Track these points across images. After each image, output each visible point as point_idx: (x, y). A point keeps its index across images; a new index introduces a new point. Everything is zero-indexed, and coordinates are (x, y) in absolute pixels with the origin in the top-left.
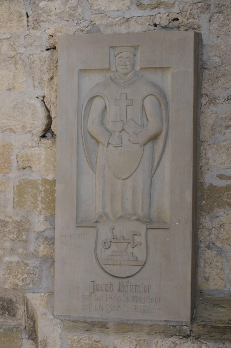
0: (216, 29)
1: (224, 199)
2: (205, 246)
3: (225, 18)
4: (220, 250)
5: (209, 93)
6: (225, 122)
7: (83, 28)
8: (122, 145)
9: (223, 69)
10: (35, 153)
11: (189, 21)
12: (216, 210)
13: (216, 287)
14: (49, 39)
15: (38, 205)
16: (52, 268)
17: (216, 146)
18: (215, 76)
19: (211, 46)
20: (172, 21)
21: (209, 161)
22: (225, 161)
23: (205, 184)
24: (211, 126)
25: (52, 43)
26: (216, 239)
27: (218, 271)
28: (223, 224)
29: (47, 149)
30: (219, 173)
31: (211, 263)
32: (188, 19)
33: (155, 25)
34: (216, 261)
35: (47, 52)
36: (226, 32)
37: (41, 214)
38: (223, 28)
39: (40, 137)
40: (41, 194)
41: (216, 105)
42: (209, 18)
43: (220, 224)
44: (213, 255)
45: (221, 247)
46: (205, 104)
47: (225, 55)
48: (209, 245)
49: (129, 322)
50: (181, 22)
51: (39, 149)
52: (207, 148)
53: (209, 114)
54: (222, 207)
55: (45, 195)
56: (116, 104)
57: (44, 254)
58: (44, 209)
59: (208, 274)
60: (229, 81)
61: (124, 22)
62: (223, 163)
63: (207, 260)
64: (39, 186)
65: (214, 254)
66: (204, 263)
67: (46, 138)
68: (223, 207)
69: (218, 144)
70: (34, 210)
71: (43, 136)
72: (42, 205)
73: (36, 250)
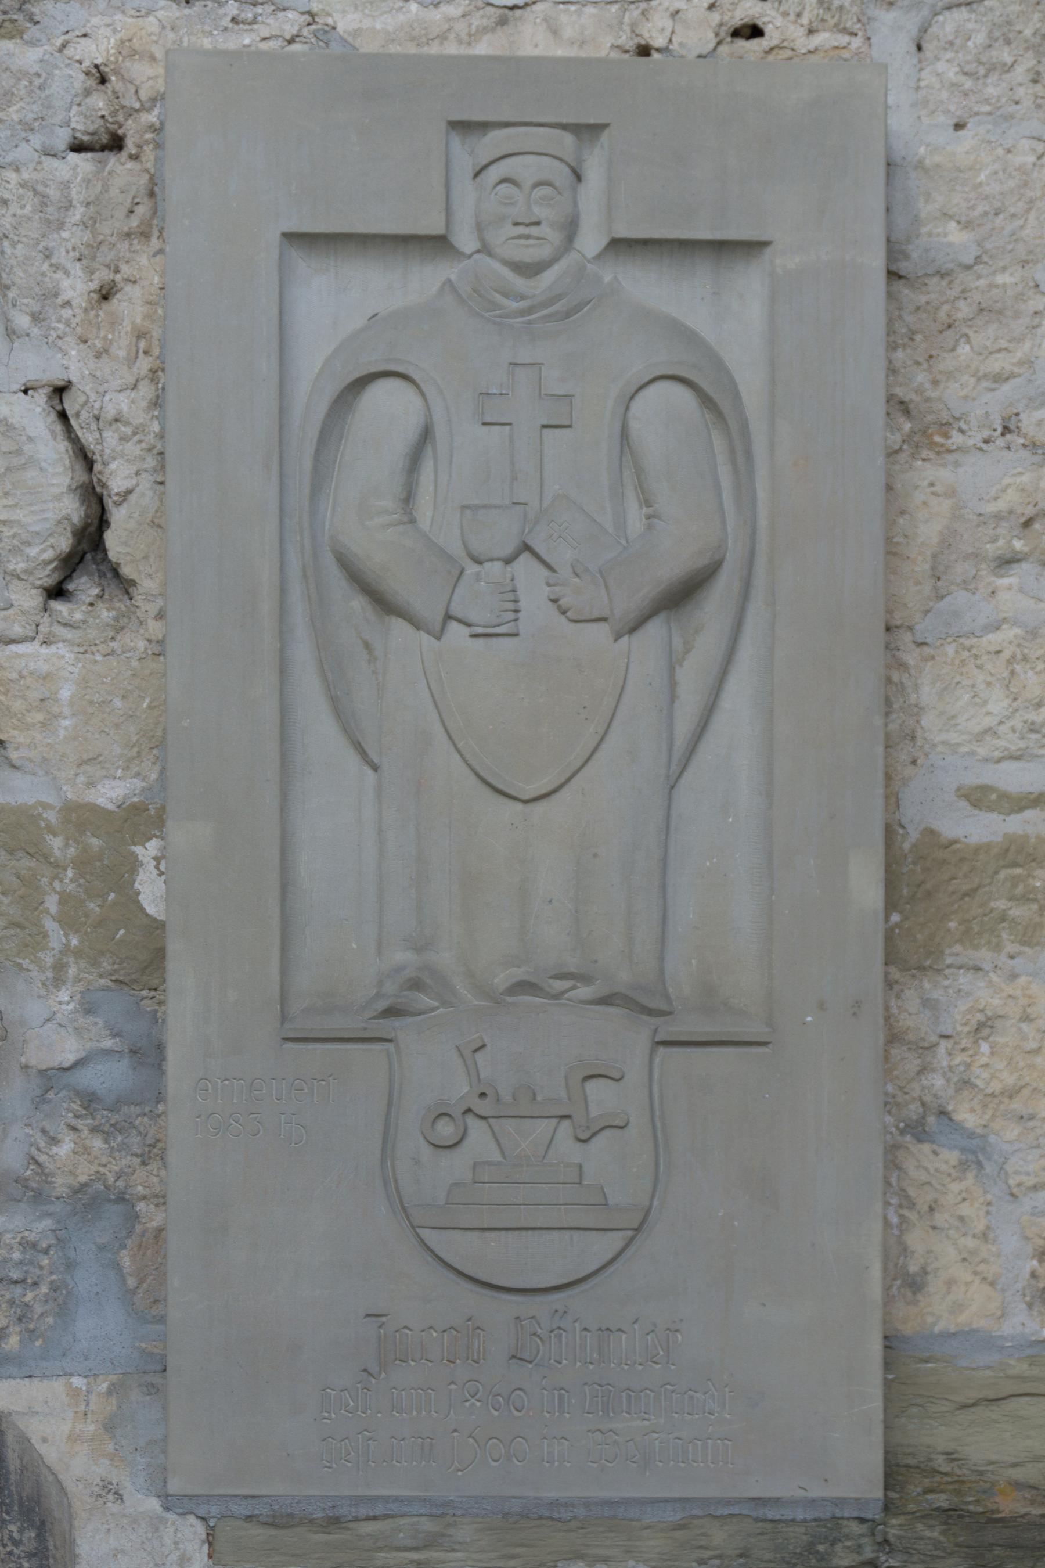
0: (953, 85)
1: (992, 904)
2: (902, 1125)
3: (997, 34)
4: (974, 1142)
5: (914, 396)
6: (994, 540)
7: (272, 45)
8: (517, 626)
9: (982, 283)
10: (25, 673)
11: (817, 40)
12: (957, 955)
13: (962, 1318)
14: (87, 93)
15: (45, 935)
16: (125, 1248)
17: (957, 652)
18: (942, 315)
19: (926, 171)
20: (729, 39)
21: (918, 722)
22: (1001, 723)
23: (901, 831)
24: (929, 553)
25: (103, 117)
26: (956, 1091)
27: (971, 1243)
28: (989, 1019)
29: (85, 652)
30: (971, 780)
31: (934, 1206)
32: (811, 32)
33: (644, 51)
34: (960, 1198)
35: (73, 157)
36: (998, 101)
37: (58, 981)
38: (985, 85)
39: (45, 594)
40: (61, 881)
41: (950, 458)
42: (915, 32)
43: (974, 1023)
44: (944, 1167)
45: (979, 1131)
46: (897, 447)
47: (997, 214)
48: (921, 1121)
49: (566, 1515)
50: (775, 42)
51: (44, 650)
52: (912, 663)
53: (919, 497)
54: (983, 942)
55: (80, 885)
56: (488, 419)
57: (83, 1179)
58: (78, 953)
59: (922, 1261)
60: (1009, 341)
61: (485, 28)
62: (990, 729)
63: (912, 1192)
64: (49, 838)
65: (947, 1162)
66: (900, 1206)
67: (70, 602)
68: (989, 942)
69: (961, 640)
70: (25, 963)
71: (57, 592)
72: (66, 935)
73: (37, 1163)
